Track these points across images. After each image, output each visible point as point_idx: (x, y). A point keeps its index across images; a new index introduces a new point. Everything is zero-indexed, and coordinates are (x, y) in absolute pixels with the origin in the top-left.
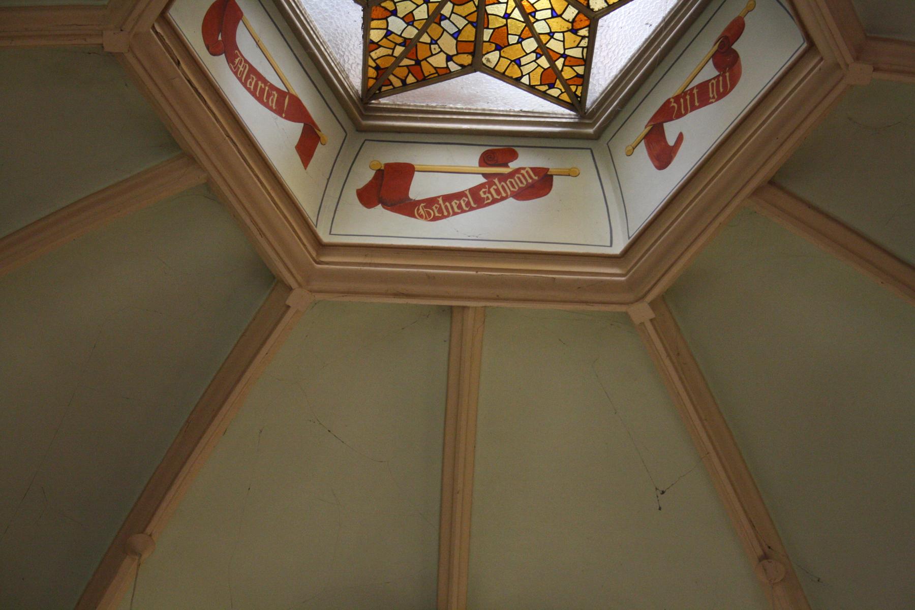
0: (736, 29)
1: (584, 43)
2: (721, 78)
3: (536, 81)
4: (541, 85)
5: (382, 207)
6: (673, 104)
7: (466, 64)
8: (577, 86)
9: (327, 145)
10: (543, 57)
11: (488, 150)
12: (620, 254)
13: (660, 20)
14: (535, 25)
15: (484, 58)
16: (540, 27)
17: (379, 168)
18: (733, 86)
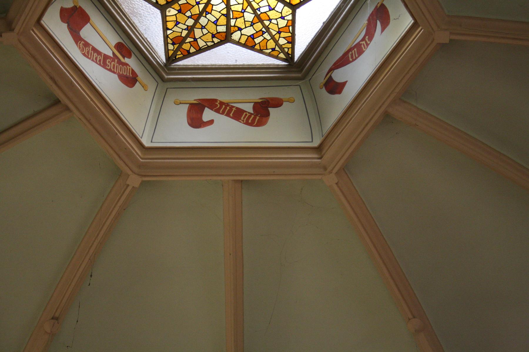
0: (277, 103)
1: (210, 44)
2: (253, 116)
3: (171, 36)
4: (171, 40)
5: (67, 26)
6: (217, 103)
7: (159, 3)
8: (182, 54)
11: (122, 43)
12: (146, 147)
13: (241, 63)
14: (202, 17)
15: (170, 8)
16: (203, 21)
17: (76, 5)
18: (257, 125)
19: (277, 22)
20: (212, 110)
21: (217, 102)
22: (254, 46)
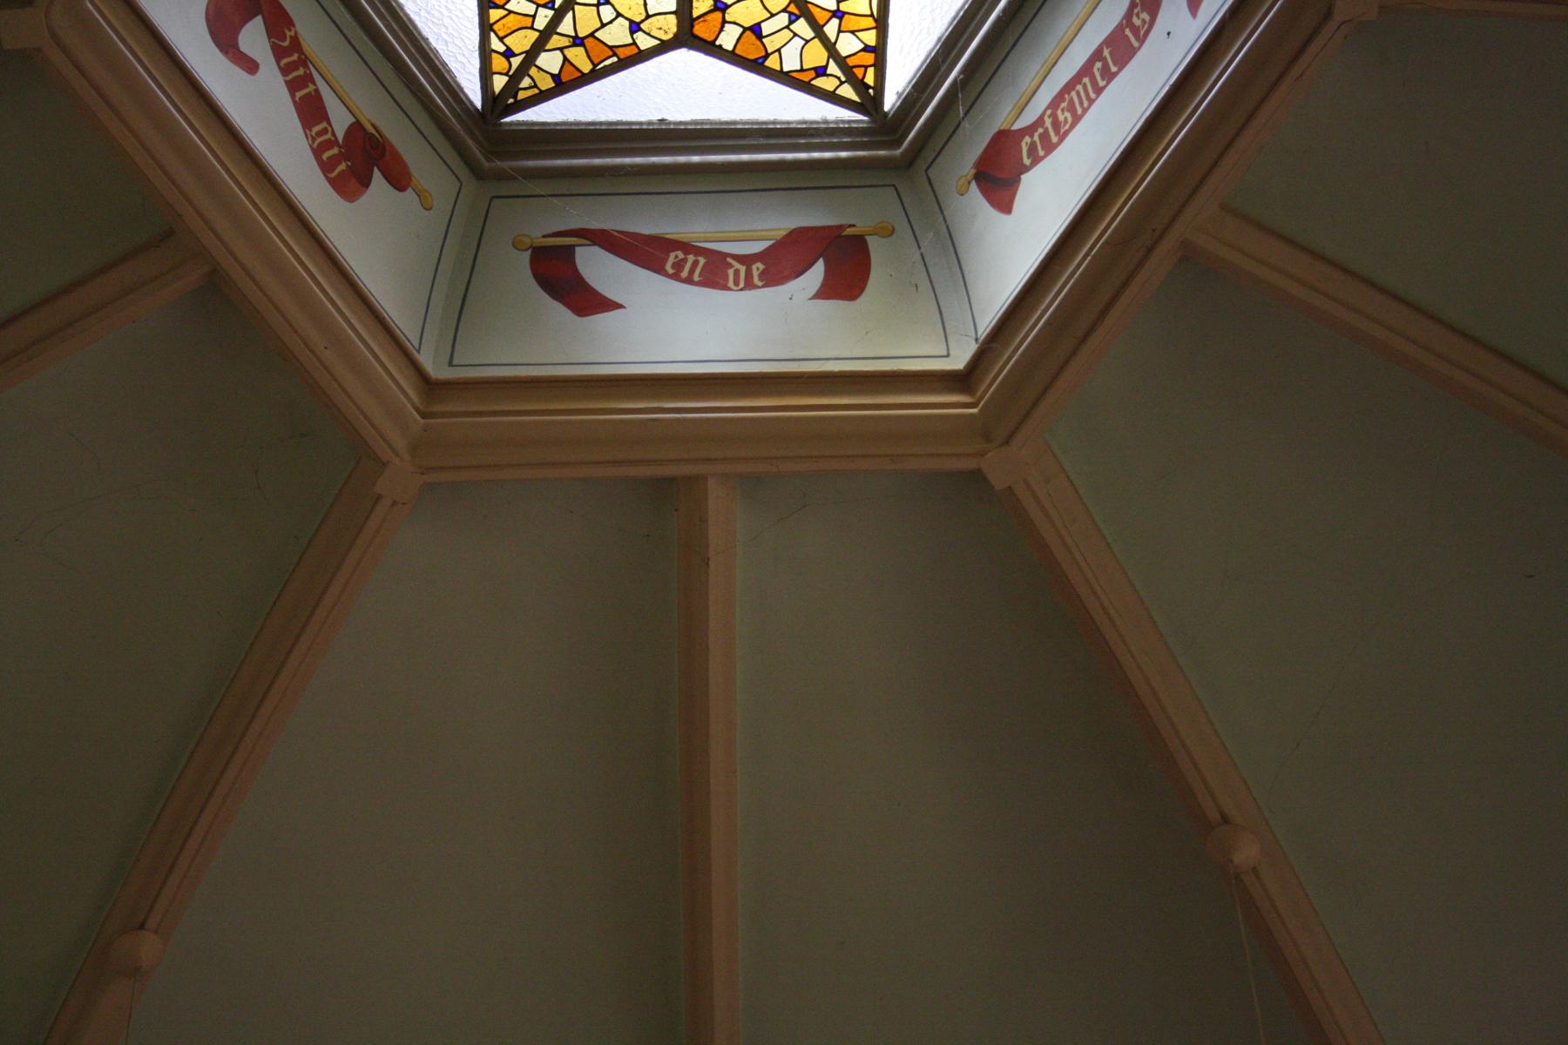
0: (399, 179)
2: (335, 151)
5: (351, 122)
6: (288, 33)
9: (434, 208)
10: (802, 21)
19: (611, 22)
20: (269, 38)
21: (290, 30)
22: (492, 5)
